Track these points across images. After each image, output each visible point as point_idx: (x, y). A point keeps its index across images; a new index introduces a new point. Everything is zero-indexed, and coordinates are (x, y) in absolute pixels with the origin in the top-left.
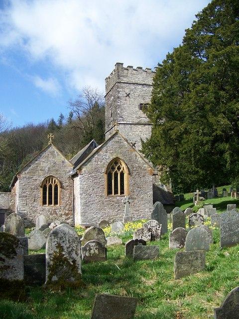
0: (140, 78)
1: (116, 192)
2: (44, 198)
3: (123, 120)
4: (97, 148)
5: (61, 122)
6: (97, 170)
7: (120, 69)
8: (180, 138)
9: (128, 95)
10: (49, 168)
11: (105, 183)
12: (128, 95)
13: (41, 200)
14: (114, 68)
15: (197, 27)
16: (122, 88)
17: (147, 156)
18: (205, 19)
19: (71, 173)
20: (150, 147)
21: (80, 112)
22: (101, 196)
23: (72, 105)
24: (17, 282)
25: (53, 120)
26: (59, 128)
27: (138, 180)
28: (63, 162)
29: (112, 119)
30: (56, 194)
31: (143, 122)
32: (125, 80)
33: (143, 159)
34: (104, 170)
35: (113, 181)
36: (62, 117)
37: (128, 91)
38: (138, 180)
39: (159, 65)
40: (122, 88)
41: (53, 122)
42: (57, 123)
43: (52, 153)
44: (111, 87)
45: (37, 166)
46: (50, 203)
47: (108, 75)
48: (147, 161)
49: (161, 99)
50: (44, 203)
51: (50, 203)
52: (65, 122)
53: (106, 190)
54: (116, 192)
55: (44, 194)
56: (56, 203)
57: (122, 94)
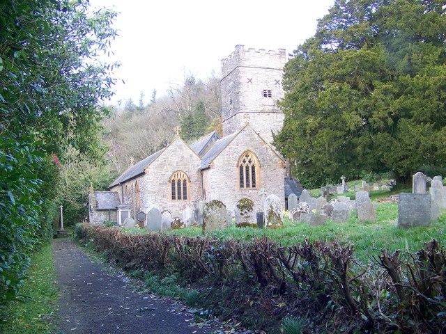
0: (265, 61)
1: (248, 186)
2: (173, 193)
3: (246, 109)
7: (241, 50)
8: (314, 132)
9: (250, 81)
10: (177, 163)
11: (238, 176)
12: (250, 81)
14: (234, 50)
15: (328, 19)
17: (279, 149)
18: (334, 13)
20: (282, 140)
26: (141, 110)
28: (191, 156)
29: (231, 106)
30: (185, 189)
31: (267, 110)
33: (274, 152)
35: (182, 192)
44: (229, 70)
47: (226, 55)
48: (277, 152)
49: (297, 313)
50: (174, 198)
54: (248, 186)
55: (173, 189)
56: (185, 198)
57: (243, 80)
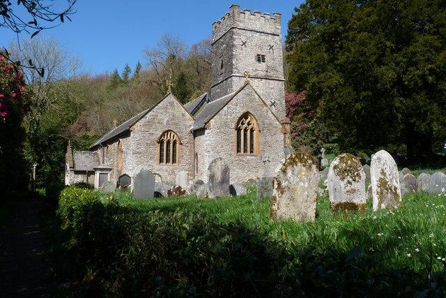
1: (245, 151)
2: (161, 155)
3: (239, 73)
4: (230, 95)
5: (126, 75)
6: (226, 124)
10: (168, 121)
12: (244, 44)
13: (158, 157)
16: (238, 34)
19: (192, 127)
21: (158, 64)
22: (231, 155)
23: (150, 55)
24: (413, 271)
25: (116, 72)
27: (269, 138)
28: (183, 115)
31: (259, 76)
32: (241, 25)
34: (233, 126)
36: (128, 69)
37: (244, 39)
38: (269, 138)
39: (296, 10)
40: (238, 34)
41: (116, 75)
42: (120, 74)
43: (172, 104)
45: (154, 119)
46: (168, 161)
50: (161, 161)
51: (168, 161)
52: (130, 76)
53: (235, 148)
55: (161, 150)
56: (174, 161)
